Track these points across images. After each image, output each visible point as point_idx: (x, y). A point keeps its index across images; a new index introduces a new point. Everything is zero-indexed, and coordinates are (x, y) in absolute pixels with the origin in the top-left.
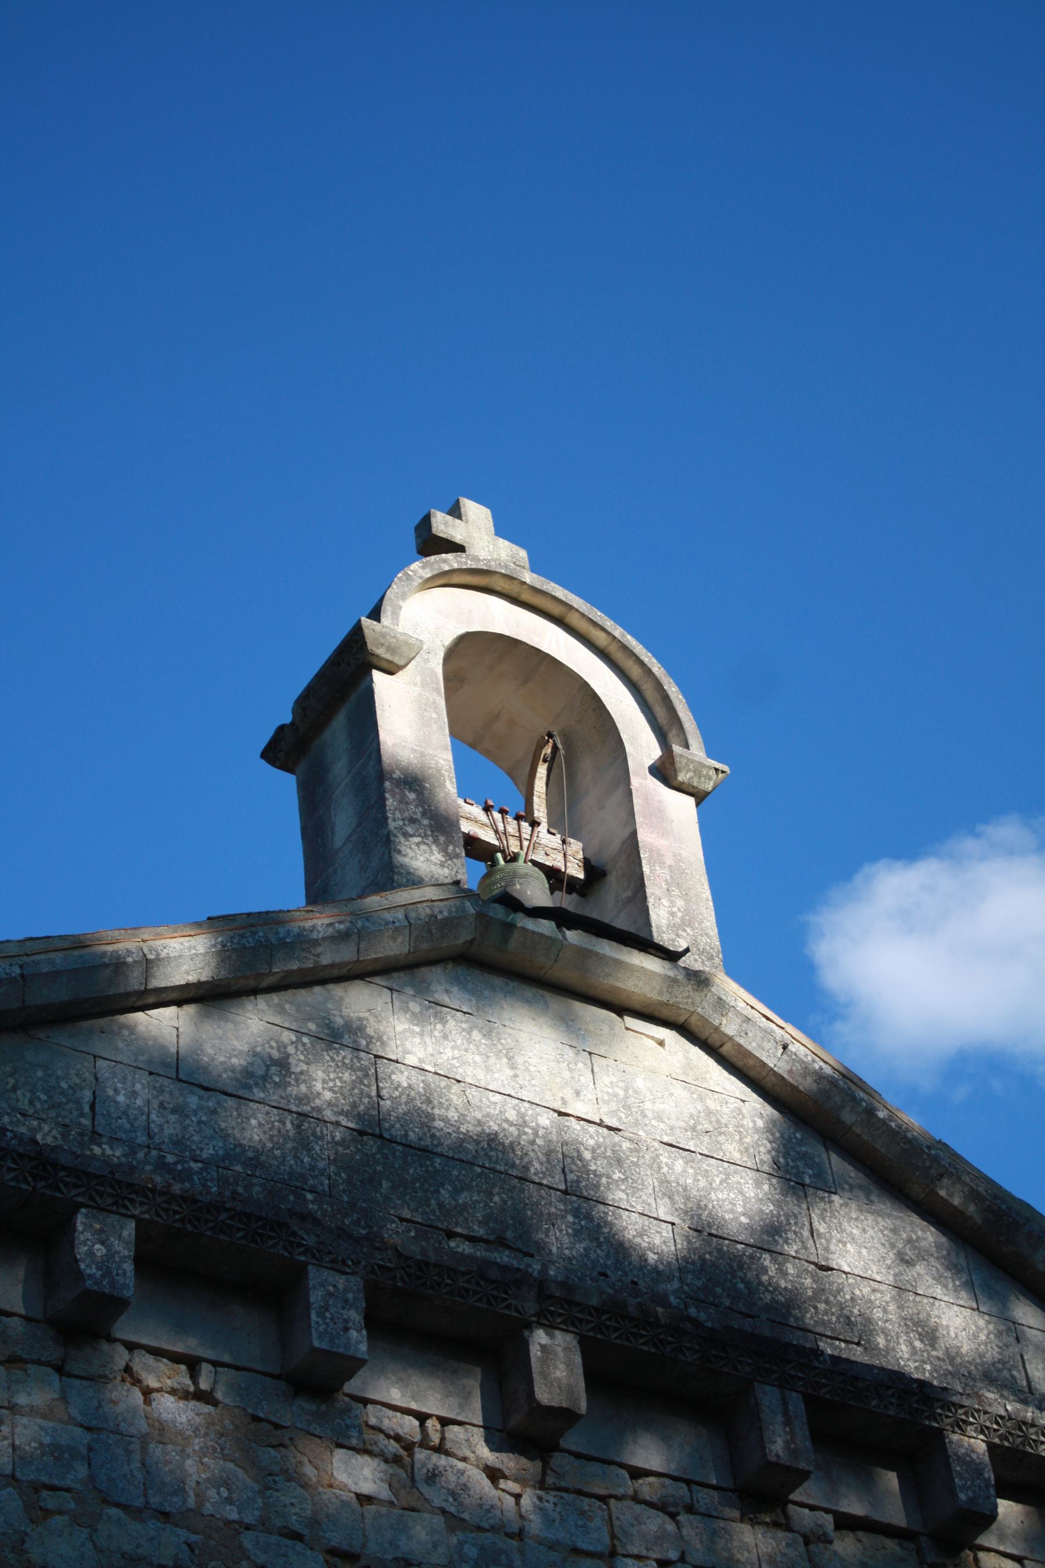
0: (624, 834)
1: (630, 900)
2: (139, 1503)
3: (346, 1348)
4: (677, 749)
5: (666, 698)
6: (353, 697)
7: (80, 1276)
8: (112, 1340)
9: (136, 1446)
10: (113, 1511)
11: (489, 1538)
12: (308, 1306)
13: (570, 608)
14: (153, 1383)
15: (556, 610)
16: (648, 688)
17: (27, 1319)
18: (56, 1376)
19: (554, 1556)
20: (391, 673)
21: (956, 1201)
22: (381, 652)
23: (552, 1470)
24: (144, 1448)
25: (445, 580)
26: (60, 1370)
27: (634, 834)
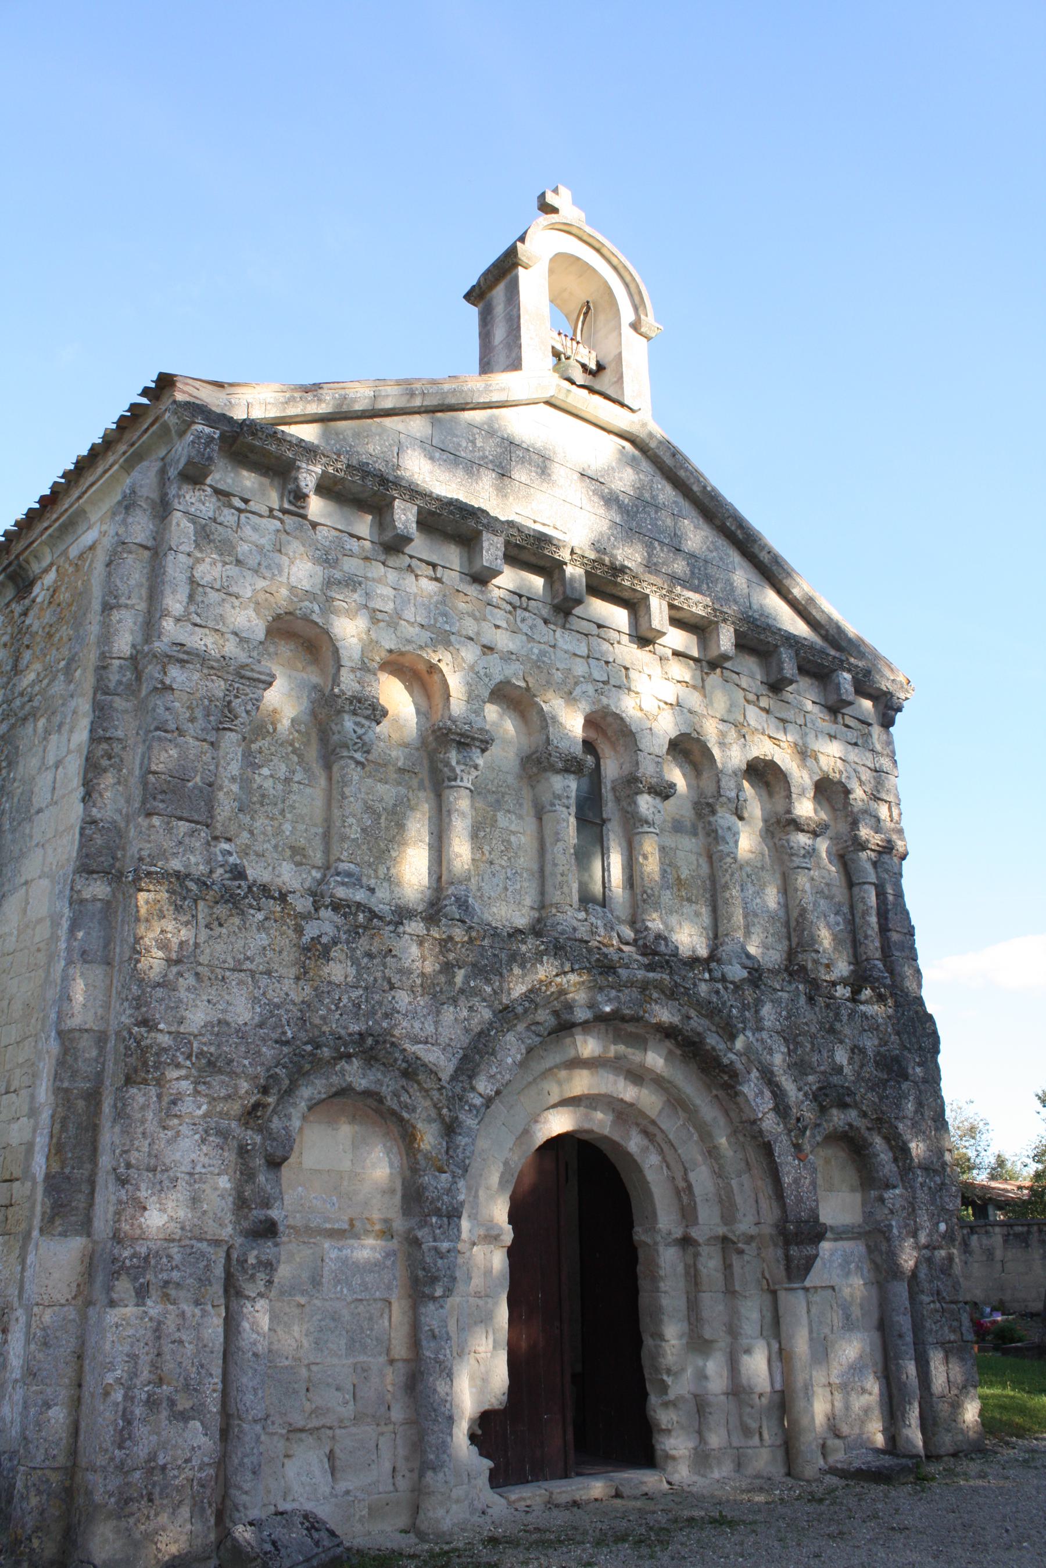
0: (617, 352)
1: (616, 382)
2: (413, 620)
3: (142, 585)
4: (643, 317)
5: (640, 293)
6: (508, 278)
7: (395, 527)
8: (403, 553)
9: (412, 598)
10: (402, 622)
11: (543, 646)
12: (482, 548)
13: (603, 245)
14: (420, 573)
15: (597, 245)
16: (632, 286)
17: (372, 542)
18: (382, 566)
19: (567, 656)
20: (526, 268)
21: (733, 528)
22: (524, 259)
23: (27, 891)
24: (415, 599)
25: (553, 227)
26: (384, 564)
27: (620, 354)
